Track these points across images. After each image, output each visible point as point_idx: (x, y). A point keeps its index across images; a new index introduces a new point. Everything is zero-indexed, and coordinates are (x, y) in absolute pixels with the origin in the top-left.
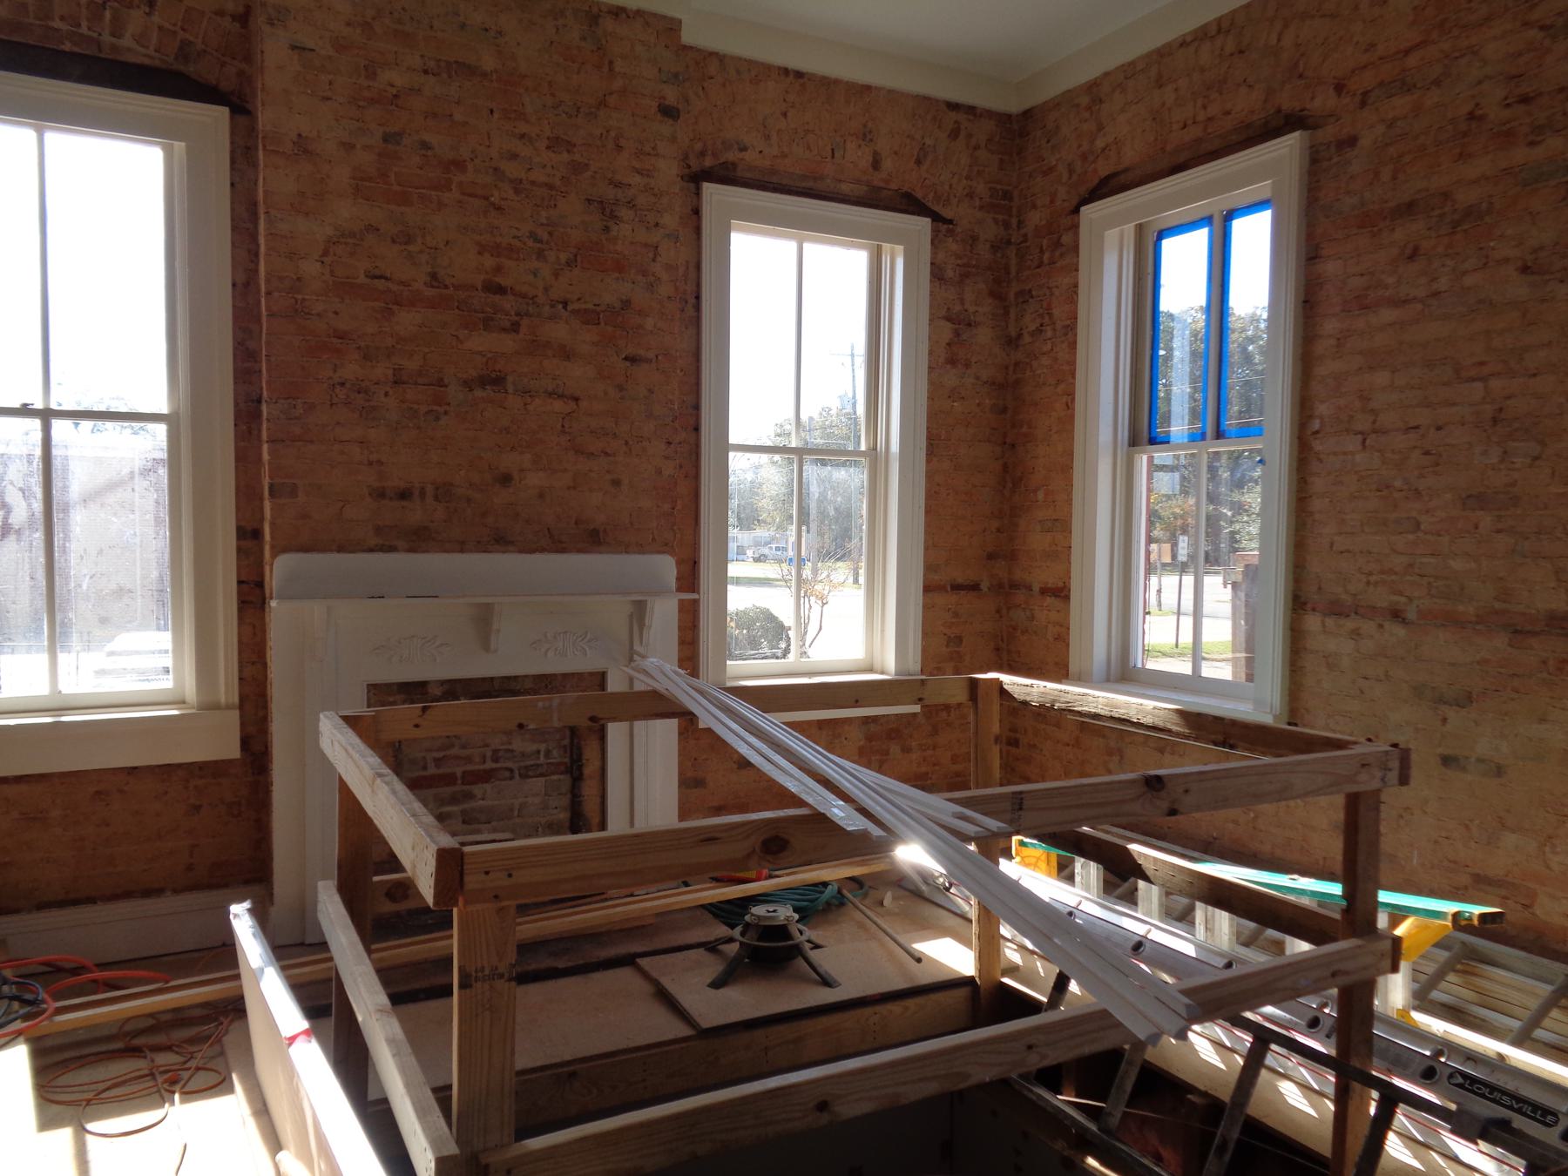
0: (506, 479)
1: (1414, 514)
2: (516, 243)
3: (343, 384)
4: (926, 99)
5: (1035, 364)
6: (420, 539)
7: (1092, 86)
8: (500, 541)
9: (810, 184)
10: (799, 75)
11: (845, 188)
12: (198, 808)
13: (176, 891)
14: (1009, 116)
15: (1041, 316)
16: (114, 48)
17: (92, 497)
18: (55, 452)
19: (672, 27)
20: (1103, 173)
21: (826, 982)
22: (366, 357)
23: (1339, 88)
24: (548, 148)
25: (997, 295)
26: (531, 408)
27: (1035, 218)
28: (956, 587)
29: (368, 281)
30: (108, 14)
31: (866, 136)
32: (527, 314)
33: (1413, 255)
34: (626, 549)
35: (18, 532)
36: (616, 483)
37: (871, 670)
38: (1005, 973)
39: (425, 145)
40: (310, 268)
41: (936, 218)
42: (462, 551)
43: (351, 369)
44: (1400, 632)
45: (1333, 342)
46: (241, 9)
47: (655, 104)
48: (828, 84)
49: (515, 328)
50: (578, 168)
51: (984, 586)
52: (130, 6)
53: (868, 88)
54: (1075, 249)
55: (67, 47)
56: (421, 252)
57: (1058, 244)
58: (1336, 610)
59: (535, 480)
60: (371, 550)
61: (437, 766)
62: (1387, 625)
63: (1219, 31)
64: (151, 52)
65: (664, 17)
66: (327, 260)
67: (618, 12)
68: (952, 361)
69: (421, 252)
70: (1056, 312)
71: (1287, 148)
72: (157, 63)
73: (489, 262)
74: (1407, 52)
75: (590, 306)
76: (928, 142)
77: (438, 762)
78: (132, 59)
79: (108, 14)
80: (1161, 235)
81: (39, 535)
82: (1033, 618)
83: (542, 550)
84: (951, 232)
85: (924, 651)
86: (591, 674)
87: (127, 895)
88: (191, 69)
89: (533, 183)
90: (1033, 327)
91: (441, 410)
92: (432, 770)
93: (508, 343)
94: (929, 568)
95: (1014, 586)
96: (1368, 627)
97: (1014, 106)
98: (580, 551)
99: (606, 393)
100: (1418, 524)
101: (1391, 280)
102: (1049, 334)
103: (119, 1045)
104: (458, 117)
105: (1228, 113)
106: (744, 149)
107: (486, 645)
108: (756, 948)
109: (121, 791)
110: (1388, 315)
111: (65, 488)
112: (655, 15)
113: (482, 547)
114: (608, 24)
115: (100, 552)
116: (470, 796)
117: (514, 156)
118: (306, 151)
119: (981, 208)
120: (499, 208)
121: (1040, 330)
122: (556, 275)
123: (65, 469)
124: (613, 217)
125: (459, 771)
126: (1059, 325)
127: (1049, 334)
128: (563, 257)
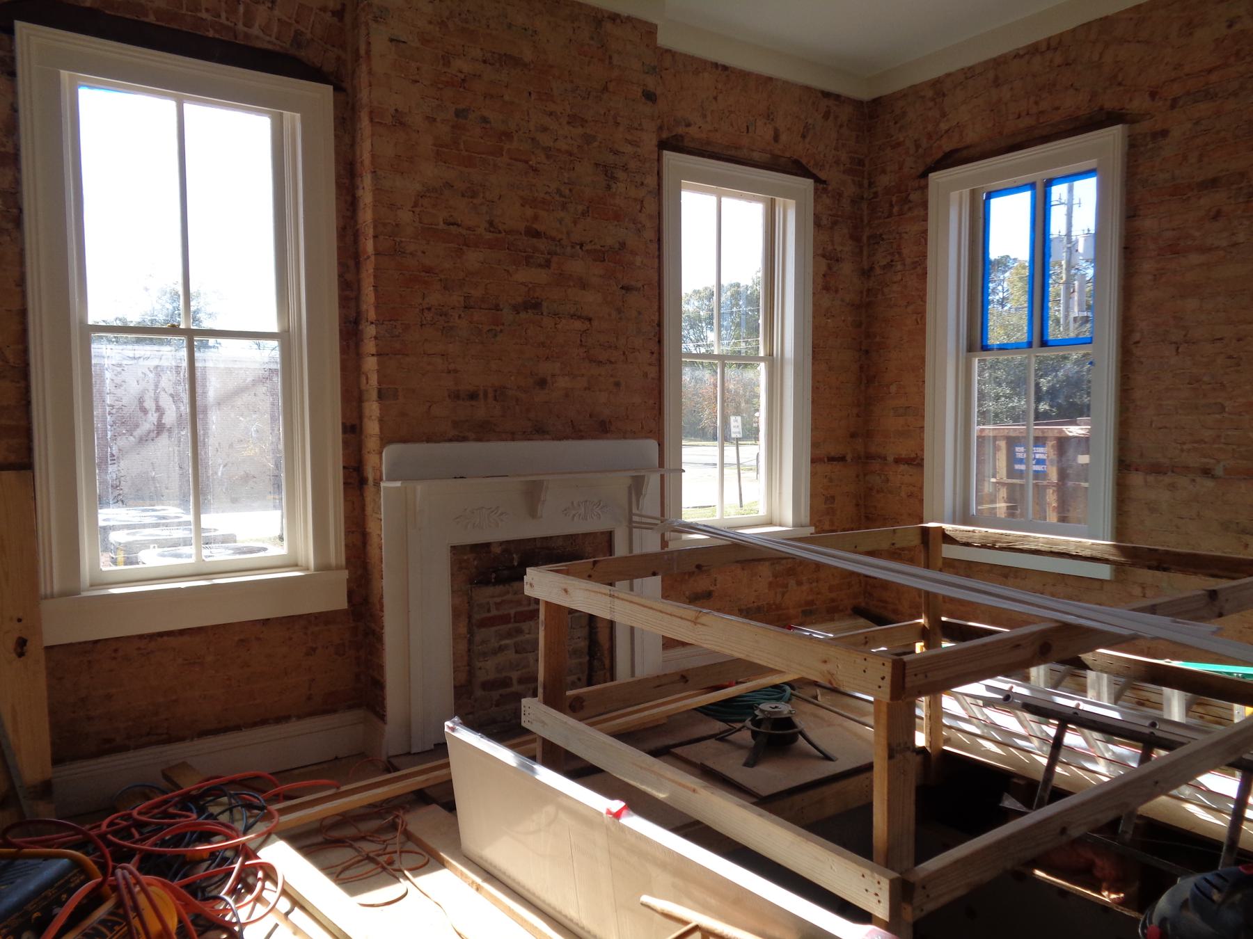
0: (542, 383)
1: (1219, 400)
2: (548, 197)
3: (429, 309)
4: (808, 89)
5: (886, 290)
6: (484, 431)
7: (936, 84)
8: (539, 431)
9: (733, 153)
10: (725, 68)
11: (756, 156)
12: (314, 649)
13: (299, 717)
14: (861, 102)
15: (892, 254)
16: (247, 36)
17: (226, 399)
18: (197, 364)
19: (650, 31)
20: (947, 149)
21: (827, 758)
22: (445, 288)
23: (1153, 95)
24: (569, 123)
25: (856, 238)
26: (559, 326)
27: (885, 181)
28: (831, 459)
29: (446, 227)
30: (241, 9)
31: (769, 116)
32: (556, 254)
33: (1217, 216)
34: (624, 435)
35: (170, 430)
36: (617, 384)
37: (770, 524)
38: (947, 741)
39: (485, 120)
40: (405, 216)
41: (817, 180)
42: (513, 440)
43: (435, 298)
44: (1210, 483)
45: (1150, 277)
46: (339, 7)
47: (640, 90)
48: (744, 75)
49: (547, 264)
50: (588, 139)
51: (849, 458)
52: (258, 3)
53: (770, 79)
54: (925, 205)
55: (211, 34)
56: (482, 204)
57: (906, 200)
58: (1157, 469)
59: (563, 382)
60: (450, 440)
61: (497, 609)
62: (1198, 479)
63: (1048, 48)
64: (273, 39)
65: (646, 22)
66: (417, 210)
67: (614, 17)
68: (826, 288)
69: (482, 204)
70: (905, 252)
71: (1113, 136)
72: (277, 49)
73: (529, 212)
74: (1210, 71)
75: (598, 247)
76: (810, 121)
77: (498, 605)
78: (259, 45)
79: (241, 9)
80: (990, 195)
81: (186, 433)
82: (888, 480)
83: (567, 438)
84: (825, 190)
85: (811, 507)
86: (602, 533)
87: (263, 722)
88: (302, 54)
89: (559, 150)
90: (884, 262)
91: (498, 329)
92: (494, 612)
93: (542, 276)
94: (815, 445)
95: (869, 457)
96: (1183, 481)
97: (865, 95)
98: (593, 438)
99: (610, 315)
100: (1223, 407)
101: (1197, 234)
102: (899, 267)
103: (320, 839)
104: (507, 98)
105: (1057, 108)
106: (688, 125)
107: (533, 513)
108: (770, 735)
109: (258, 639)
110: (1195, 258)
111: (205, 393)
112: (639, 21)
113: (527, 436)
114: (608, 26)
115: (231, 446)
116: (519, 631)
117: (545, 129)
118: (401, 123)
119: (844, 172)
120: (535, 170)
121: (890, 265)
122: (575, 223)
123: (204, 379)
124: (613, 178)
125: (512, 612)
126: (908, 261)
127: (899, 267)
128: (580, 208)
